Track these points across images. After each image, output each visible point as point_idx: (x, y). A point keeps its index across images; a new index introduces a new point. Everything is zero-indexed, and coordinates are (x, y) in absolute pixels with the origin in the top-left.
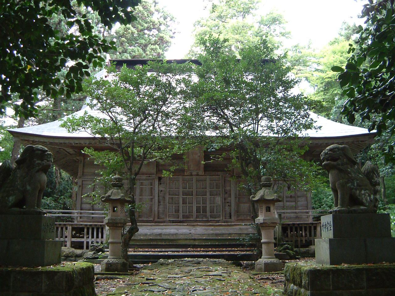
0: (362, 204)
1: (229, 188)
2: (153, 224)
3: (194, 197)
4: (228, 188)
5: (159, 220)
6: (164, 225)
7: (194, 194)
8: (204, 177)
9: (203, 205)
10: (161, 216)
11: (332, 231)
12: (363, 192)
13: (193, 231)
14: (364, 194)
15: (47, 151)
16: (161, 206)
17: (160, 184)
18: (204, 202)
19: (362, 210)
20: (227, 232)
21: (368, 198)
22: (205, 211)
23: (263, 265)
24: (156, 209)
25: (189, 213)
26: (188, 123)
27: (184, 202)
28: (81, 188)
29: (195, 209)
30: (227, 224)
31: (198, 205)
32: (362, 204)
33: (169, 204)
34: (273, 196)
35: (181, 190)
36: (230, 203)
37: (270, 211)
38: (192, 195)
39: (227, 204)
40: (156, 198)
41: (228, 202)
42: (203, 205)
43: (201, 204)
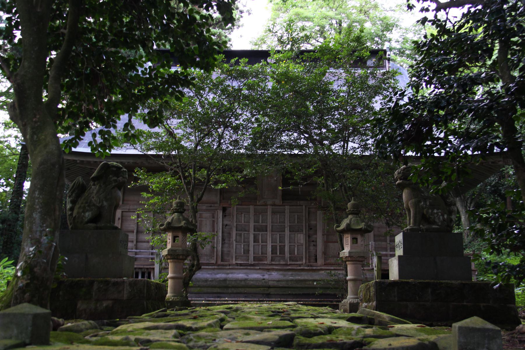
0: (434, 223)
1: (315, 222)
2: (215, 267)
3: (269, 234)
4: (313, 222)
5: (222, 263)
6: (230, 269)
7: (268, 229)
8: (282, 207)
9: (280, 244)
10: (226, 258)
11: (402, 249)
12: (435, 211)
13: (266, 277)
14: (437, 213)
15: (122, 168)
16: (226, 245)
17: (225, 216)
18: (282, 240)
19: (434, 228)
20: (311, 278)
21: (441, 217)
22: (282, 251)
23: (348, 306)
24: (220, 248)
25: (262, 254)
26: (262, 138)
27: (256, 240)
28: (120, 220)
29: (269, 249)
30: (311, 268)
31: (273, 244)
32: (434, 223)
33: (236, 242)
34: (362, 226)
35: (252, 225)
36: (316, 241)
37: (357, 243)
38: (267, 231)
39: (312, 244)
40: (220, 234)
41: (313, 241)
42: (280, 244)
43: (278, 242)
